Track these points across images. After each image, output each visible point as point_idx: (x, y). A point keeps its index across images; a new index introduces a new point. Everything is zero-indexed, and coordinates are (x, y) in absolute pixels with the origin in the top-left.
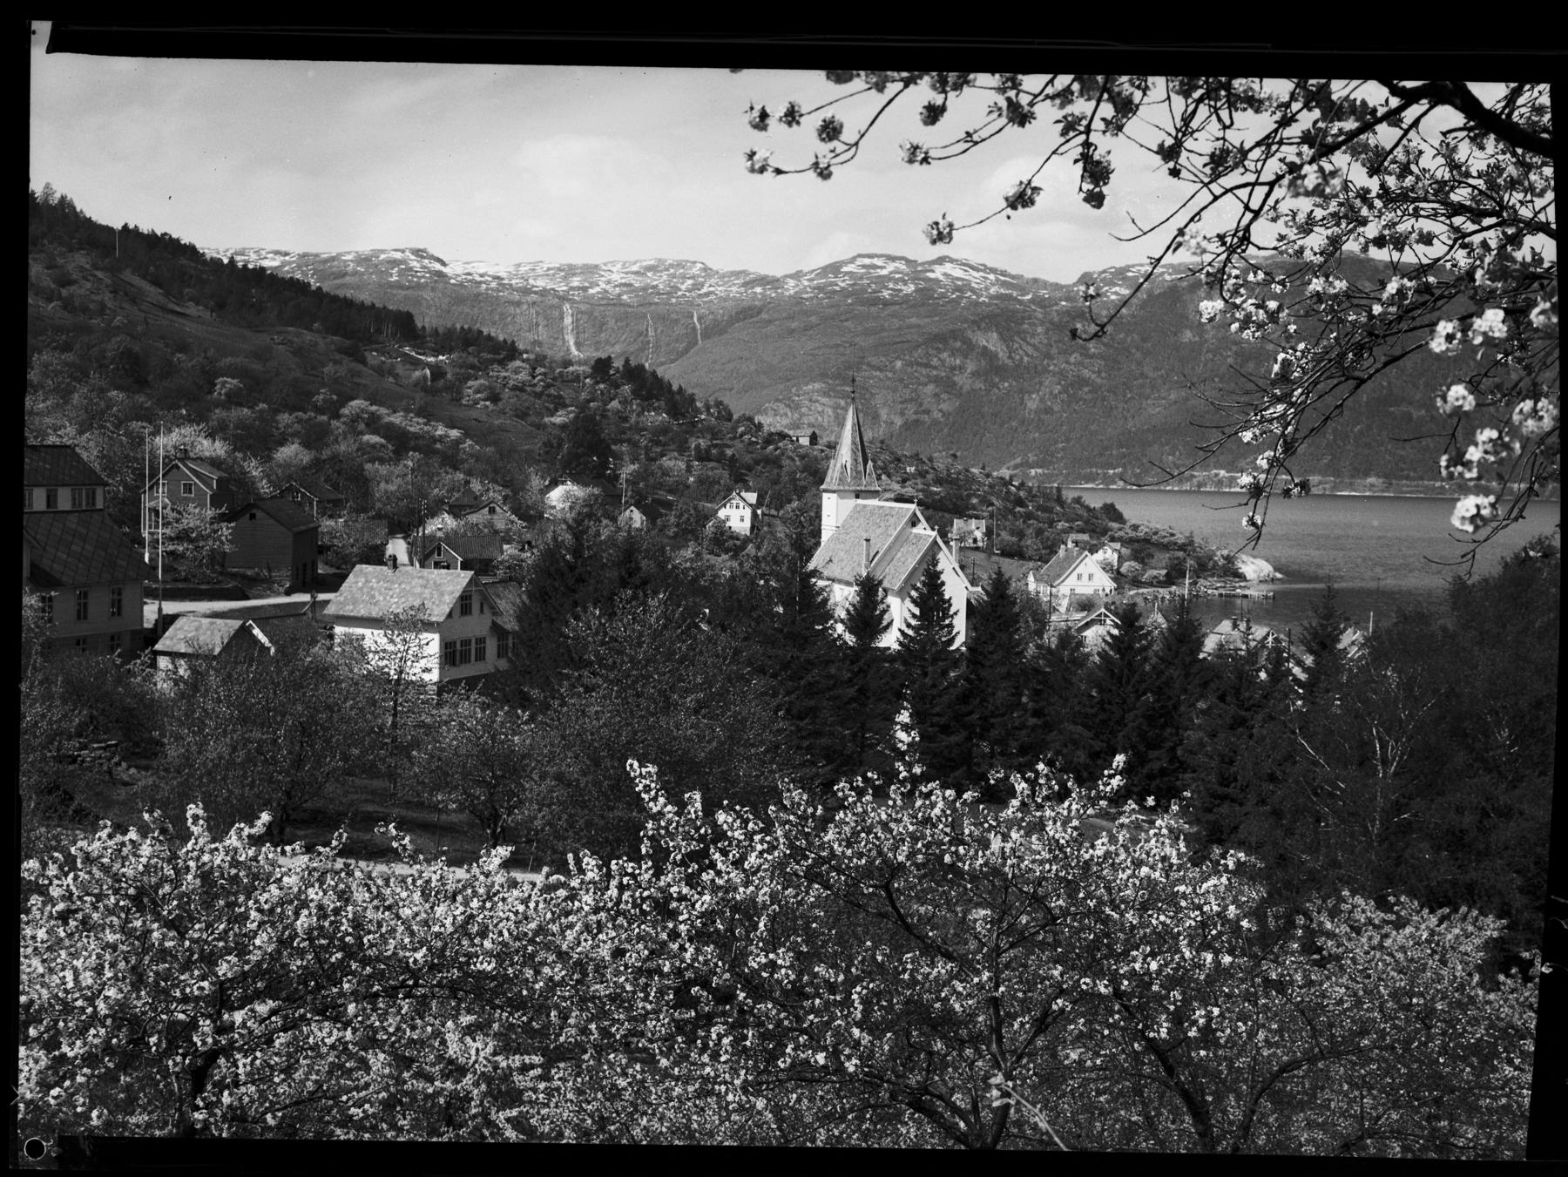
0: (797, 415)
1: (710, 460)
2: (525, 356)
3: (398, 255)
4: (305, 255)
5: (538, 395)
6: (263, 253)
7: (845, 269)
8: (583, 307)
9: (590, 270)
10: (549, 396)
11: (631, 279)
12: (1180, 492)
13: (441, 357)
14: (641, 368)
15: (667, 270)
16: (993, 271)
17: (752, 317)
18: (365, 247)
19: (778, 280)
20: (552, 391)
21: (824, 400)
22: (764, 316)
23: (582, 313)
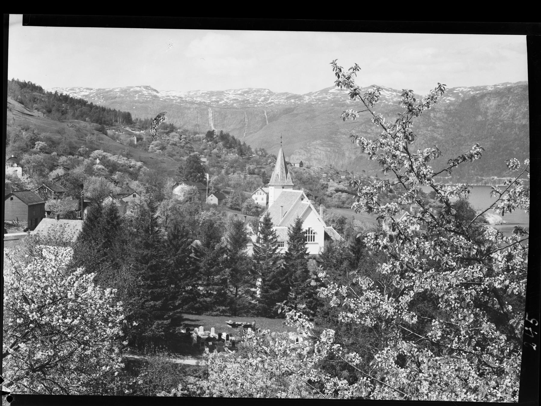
0: (309, 155)
1: (254, 174)
2: (178, 130)
3: (138, 89)
4: (99, 90)
5: (182, 147)
6: (82, 89)
7: (330, 91)
8: (217, 109)
9: (221, 93)
10: (187, 147)
11: (238, 97)
12: (477, 186)
13: (142, 132)
14: (228, 135)
15: (253, 93)
16: (395, 91)
17: (290, 112)
18: (124, 86)
19: (301, 96)
20: (188, 145)
21: (321, 148)
22: (295, 112)
23: (216, 112)
